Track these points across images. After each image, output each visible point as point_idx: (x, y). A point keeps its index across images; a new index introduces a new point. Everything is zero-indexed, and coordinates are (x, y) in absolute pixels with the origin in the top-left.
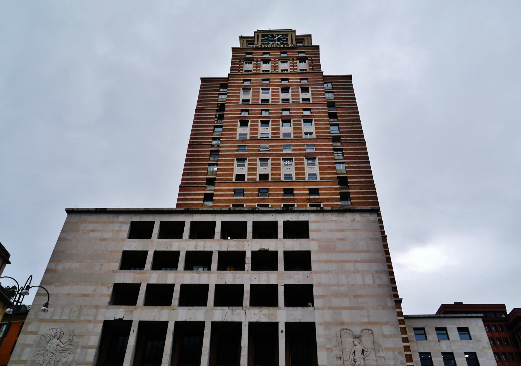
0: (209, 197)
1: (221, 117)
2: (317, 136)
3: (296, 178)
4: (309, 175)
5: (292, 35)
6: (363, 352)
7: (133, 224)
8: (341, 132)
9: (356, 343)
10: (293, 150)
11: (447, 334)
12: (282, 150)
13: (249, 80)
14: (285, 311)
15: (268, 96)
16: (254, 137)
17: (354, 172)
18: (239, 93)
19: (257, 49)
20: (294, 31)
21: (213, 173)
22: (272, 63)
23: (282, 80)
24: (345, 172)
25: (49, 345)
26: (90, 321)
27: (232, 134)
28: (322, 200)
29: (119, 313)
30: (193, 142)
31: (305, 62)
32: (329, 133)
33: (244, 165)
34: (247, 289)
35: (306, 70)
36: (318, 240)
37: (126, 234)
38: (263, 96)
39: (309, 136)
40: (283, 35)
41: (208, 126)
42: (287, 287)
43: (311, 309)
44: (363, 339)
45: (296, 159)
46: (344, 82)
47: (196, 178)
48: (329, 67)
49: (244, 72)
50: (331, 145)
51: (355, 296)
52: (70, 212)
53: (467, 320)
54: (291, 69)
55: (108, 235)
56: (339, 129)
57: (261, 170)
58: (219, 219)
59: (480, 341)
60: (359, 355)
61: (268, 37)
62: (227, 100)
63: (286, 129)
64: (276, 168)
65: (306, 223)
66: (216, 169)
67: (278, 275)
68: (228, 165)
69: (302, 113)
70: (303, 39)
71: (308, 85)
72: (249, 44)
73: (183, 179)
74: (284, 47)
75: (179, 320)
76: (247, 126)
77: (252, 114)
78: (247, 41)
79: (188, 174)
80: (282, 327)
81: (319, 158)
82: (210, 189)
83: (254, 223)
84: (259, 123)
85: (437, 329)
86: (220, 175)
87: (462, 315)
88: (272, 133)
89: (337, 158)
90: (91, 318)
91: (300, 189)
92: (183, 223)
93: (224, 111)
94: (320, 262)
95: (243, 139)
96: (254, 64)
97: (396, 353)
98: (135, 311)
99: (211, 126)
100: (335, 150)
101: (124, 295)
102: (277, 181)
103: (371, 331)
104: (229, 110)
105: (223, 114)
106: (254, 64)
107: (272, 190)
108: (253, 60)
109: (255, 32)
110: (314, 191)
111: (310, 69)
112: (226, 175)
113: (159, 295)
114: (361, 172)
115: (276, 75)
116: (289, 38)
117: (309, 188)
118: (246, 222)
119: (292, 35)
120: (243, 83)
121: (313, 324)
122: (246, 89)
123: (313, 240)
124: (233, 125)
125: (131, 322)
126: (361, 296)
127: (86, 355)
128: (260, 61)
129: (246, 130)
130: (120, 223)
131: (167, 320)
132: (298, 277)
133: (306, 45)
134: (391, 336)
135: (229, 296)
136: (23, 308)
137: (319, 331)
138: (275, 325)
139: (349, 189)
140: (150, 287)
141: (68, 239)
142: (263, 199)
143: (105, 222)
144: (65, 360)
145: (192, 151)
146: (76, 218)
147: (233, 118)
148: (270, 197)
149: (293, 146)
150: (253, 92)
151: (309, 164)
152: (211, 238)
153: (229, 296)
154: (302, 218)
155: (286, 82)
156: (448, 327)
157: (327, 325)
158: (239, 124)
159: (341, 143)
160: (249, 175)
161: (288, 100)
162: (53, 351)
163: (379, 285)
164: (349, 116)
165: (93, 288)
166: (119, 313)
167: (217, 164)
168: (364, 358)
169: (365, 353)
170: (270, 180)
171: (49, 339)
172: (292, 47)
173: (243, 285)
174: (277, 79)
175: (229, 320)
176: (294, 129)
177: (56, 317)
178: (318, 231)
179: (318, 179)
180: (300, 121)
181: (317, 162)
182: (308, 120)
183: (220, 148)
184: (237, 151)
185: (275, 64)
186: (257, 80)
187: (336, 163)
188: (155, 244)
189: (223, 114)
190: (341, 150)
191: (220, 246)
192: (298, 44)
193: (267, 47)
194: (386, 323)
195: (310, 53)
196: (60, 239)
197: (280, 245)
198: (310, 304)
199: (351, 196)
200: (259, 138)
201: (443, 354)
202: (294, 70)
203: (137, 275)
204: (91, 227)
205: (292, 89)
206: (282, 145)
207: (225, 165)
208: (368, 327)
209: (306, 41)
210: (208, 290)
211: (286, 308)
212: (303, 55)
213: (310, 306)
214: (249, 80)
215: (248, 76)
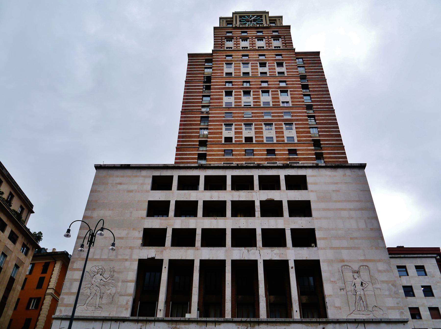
0: (202, 156)
1: (208, 88)
2: (293, 105)
3: (277, 141)
4: (267, 138)
5: (265, 16)
6: (362, 284)
7: (154, 178)
8: (312, 101)
9: (356, 277)
10: (273, 116)
11: (406, 271)
12: (263, 116)
13: (231, 56)
14: (293, 251)
15: (248, 69)
16: (238, 105)
17: (326, 136)
18: (223, 67)
19: (236, 28)
20: (268, 13)
21: (204, 136)
22: (250, 41)
23: (260, 55)
24: (318, 136)
25: (94, 279)
26: (126, 260)
27: (219, 102)
28: (300, 159)
29: (151, 252)
30: (185, 109)
31: (278, 40)
32: (303, 102)
33: (231, 129)
34: (259, 233)
35: (279, 47)
36: (316, 191)
37: (149, 186)
38: (244, 70)
39: (285, 105)
40: (258, 16)
41: (197, 96)
42: (264, 231)
43: (315, 249)
44: (361, 273)
45: (275, 125)
46: (313, 58)
47: (190, 140)
48: (301, 44)
49: (225, 49)
50: (306, 112)
51: (351, 238)
52: (98, 167)
53: (424, 260)
54: (266, 46)
55: (132, 187)
56: (311, 98)
57: (246, 133)
58: (229, 174)
59: (434, 277)
60: (359, 287)
61: (245, 17)
62: (213, 73)
63: (266, 98)
64: (259, 132)
65: (305, 177)
66: (206, 132)
67: (284, 221)
68: (218, 129)
69: (279, 84)
70: (276, 20)
71: (283, 60)
72: (228, 24)
73: (178, 141)
74: (260, 27)
75: (203, 258)
76: (231, 95)
77: (235, 85)
78: (226, 21)
79: (183, 137)
80: (291, 264)
81: (295, 124)
82: (202, 150)
83: (260, 177)
84: (242, 93)
85: (398, 267)
86: (211, 138)
87: (419, 256)
88: (254, 102)
89: (310, 123)
90: (127, 257)
91: (280, 150)
92: (198, 177)
93: (210, 82)
94: (319, 210)
95: (229, 107)
96: (234, 41)
97: (390, 285)
98: (164, 251)
99: (200, 96)
100: (309, 116)
101: (153, 238)
102: (260, 143)
103: (368, 267)
104: (215, 82)
105: (210, 86)
106: (234, 41)
107: (256, 150)
108: (233, 38)
109: (233, 13)
110: (293, 152)
111: (283, 46)
112: (216, 138)
113: (184, 238)
114: (332, 136)
115: (254, 52)
116: (264, 18)
117: (288, 149)
118: (253, 176)
119: (265, 16)
120: (225, 58)
121: (318, 262)
122: (229, 64)
123: (312, 191)
124: (219, 95)
125: (162, 260)
126: (356, 238)
127: (126, 288)
128: (239, 39)
129: (231, 99)
130: (143, 177)
131: (193, 259)
132: (301, 223)
133: (278, 25)
134: (385, 271)
135: (244, 238)
136: (43, 250)
137: (324, 267)
138: (286, 262)
139: (321, 149)
140: (175, 231)
141: (99, 191)
142: (249, 158)
143: (130, 177)
144: (109, 292)
145: (185, 117)
146: (104, 172)
147: (219, 89)
148: (255, 157)
149: (273, 113)
150: (235, 66)
151: (287, 129)
152: (221, 189)
153: (214, 238)
154: (301, 172)
155: (263, 58)
156: (407, 265)
157: (330, 262)
158: (224, 93)
159: (314, 111)
160: (236, 137)
161: (266, 73)
162: (98, 285)
163: (371, 229)
164: (319, 87)
165: (126, 232)
166: (151, 252)
167: (207, 129)
168: (363, 289)
169: (364, 285)
170: (254, 142)
171: (93, 275)
172: (267, 27)
173: (255, 230)
174: (255, 55)
175: (246, 258)
176: (273, 98)
177: (97, 257)
178: (315, 184)
179: (296, 141)
180: (277, 91)
181: (294, 127)
182: (284, 91)
183: (209, 114)
184: (224, 117)
185: (252, 42)
186: (238, 55)
187: (310, 128)
188: (174, 195)
189: (210, 86)
190: (314, 117)
191: (232, 196)
192: (271, 25)
193: (245, 27)
194: (379, 261)
195: (282, 32)
196: (92, 191)
197: (284, 195)
198: (313, 245)
199: (324, 156)
200: (243, 106)
201: (404, 287)
202: (269, 47)
203: (163, 221)
204: (118, 180)
205: (269, 63)
206: (263, 112)
207: (215, 129)
208: (365, 264)
209: (278, 21)
210: (225, 234)
211: (294, 248)
212: (277, 34)
213: (313, 247)
214: (231, 56)
215: (229, 52)
